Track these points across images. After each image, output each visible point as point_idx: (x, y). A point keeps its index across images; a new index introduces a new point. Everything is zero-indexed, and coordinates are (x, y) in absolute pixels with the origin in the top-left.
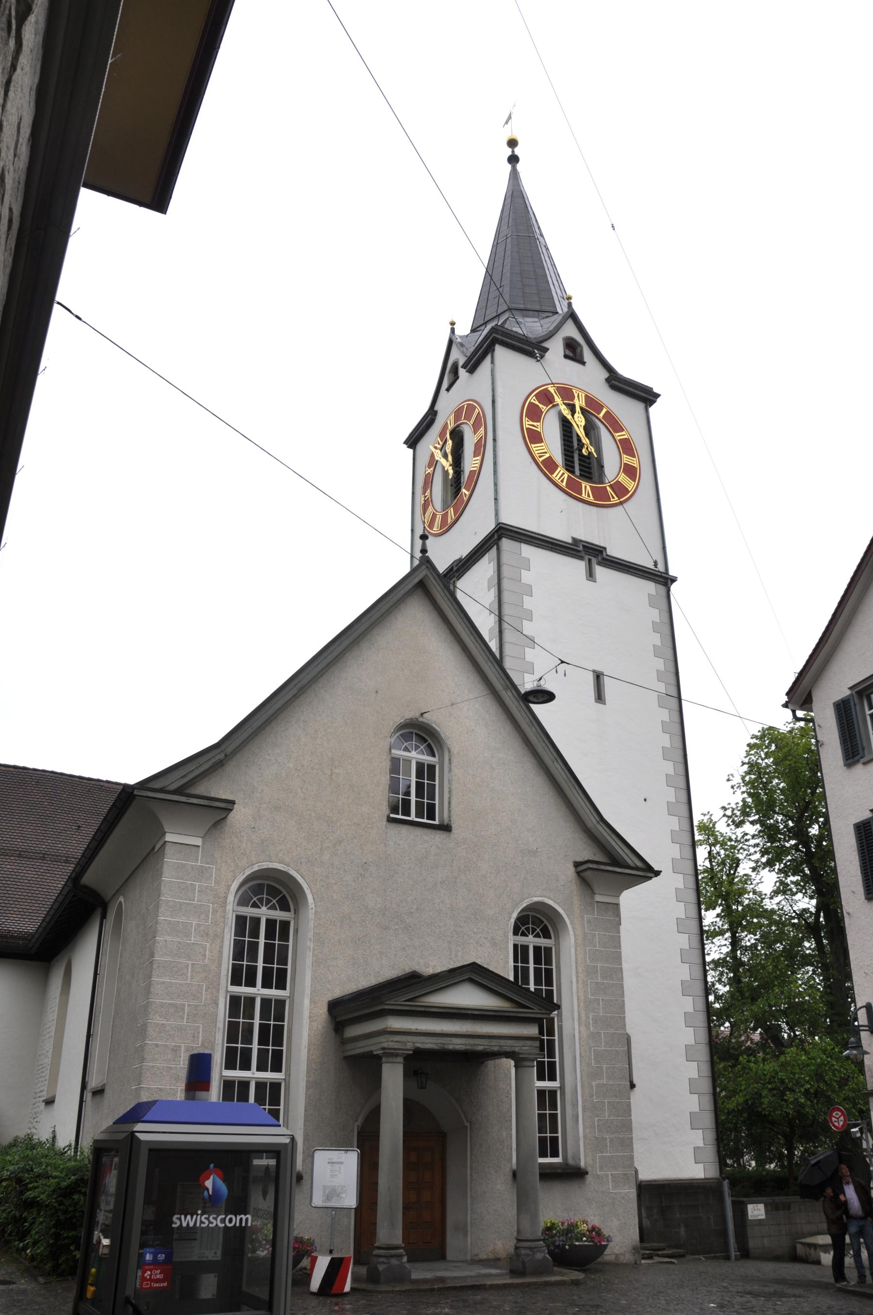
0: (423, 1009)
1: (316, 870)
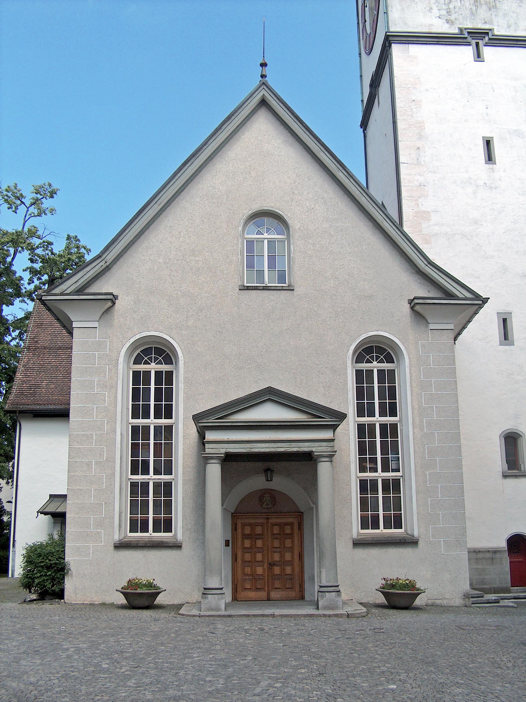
0: (230, 424)
1: (184, 332)
